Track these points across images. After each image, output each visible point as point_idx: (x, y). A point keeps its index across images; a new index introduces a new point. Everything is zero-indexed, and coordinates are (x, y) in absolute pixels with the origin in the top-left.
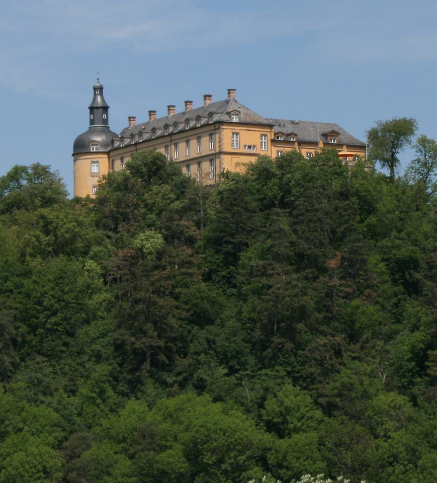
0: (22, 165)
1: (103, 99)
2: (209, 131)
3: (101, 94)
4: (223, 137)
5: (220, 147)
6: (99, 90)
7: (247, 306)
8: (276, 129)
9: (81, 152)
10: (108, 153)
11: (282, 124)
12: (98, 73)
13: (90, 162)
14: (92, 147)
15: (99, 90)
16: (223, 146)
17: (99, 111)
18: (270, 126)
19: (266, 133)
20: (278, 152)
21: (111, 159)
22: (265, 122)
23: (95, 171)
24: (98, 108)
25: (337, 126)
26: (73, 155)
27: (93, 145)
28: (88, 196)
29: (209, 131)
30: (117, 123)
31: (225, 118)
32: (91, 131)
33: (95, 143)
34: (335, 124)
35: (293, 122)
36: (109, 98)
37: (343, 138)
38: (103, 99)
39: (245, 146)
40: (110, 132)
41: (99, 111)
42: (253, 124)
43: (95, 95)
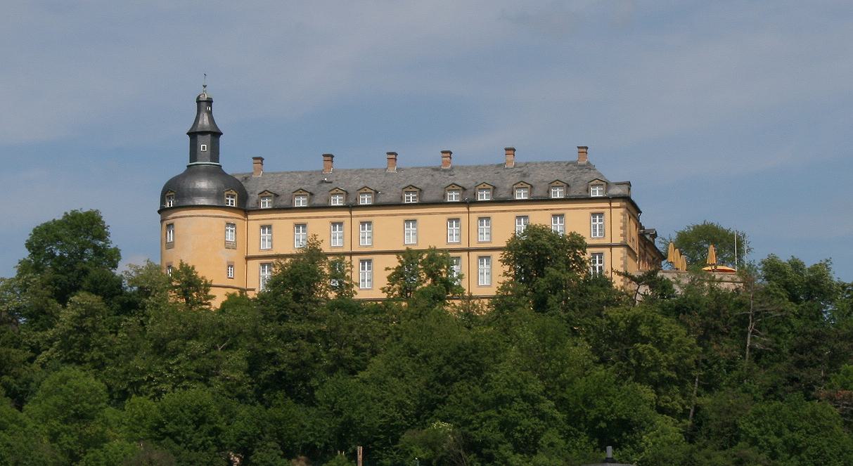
0: (86, 210)
1: (211, 119)
6: (204, 104)
9: (191, 203)
13: (445, 220)
15: (204, 104)
24: (204, 133)
26: (159, 212)
28: (24, 259)
32: (192, 171)
33: (200, 193)
38: (211, 119)
40: (224, 174)
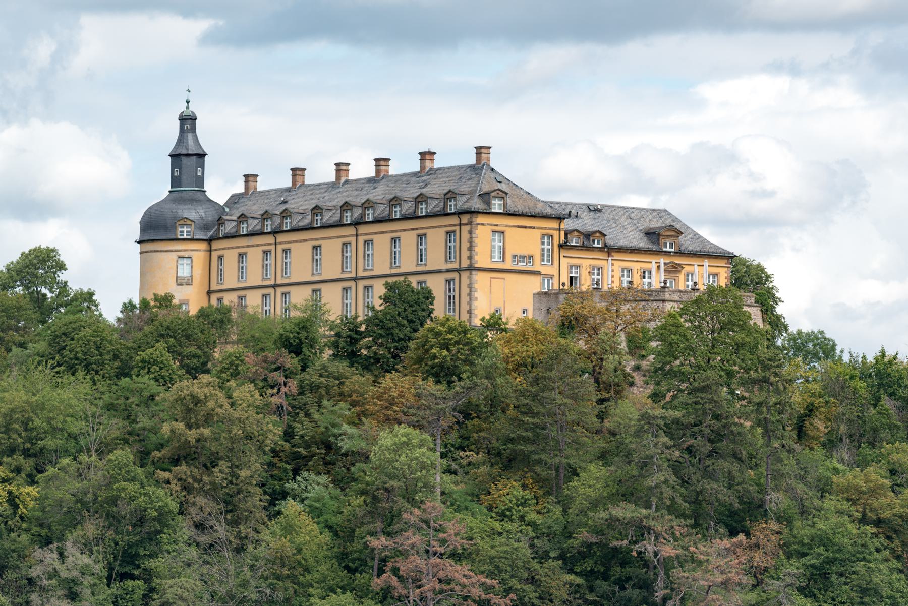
2: (446, 226)
3: (193, 129)
4: (476, 240)
5: (470, 258)
6: (187, 122)
7: (221, 472)
8: (567, 225)
9: (159, 249)
10: (209, 241)
11: (574, 213)
12: (188, 91)
14: (180, 229)
15: (187, 122)
16: (476, 258)
17: (187, 160)
18: (560, 219)
19: (551, 232)
20: (571, 267)
21: (215, 255)
22: (550, 211)
23: (185, 275)
25: (670, 214)
27: (182, 226)
29: (446, 226)
30: (219, 188)
31: (477, 204)
33: (185, 221)
34: (665, 211)
35: (595, 210)
36: (206, 135)
37: (685, 242)
39: (514, 256)
41: (187, 160)
42: (534, 217)
43: (182, 130)
